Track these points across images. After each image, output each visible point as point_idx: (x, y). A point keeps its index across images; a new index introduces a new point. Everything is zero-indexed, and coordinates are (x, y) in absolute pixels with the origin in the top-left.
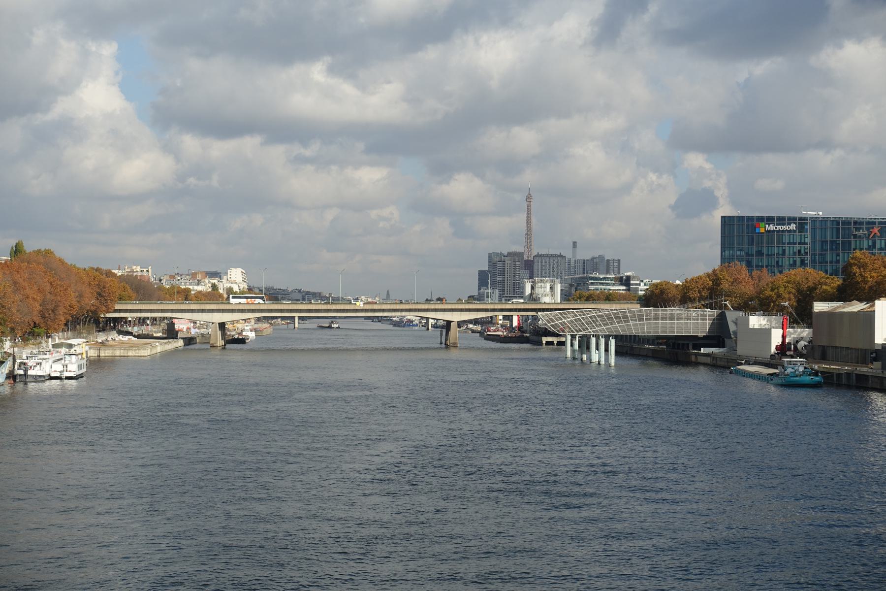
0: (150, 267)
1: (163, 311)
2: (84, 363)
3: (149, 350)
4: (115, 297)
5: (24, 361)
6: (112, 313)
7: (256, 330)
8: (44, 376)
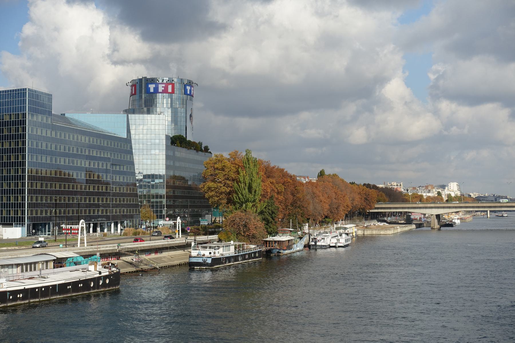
0: (402, 183)
1: (403, 208)
2: (349, 239)
3: (393, 231)
4: (375, 200)
5: (315, 237)
6: (373, 209)
7: (461, 219)
8: (326, 246)
